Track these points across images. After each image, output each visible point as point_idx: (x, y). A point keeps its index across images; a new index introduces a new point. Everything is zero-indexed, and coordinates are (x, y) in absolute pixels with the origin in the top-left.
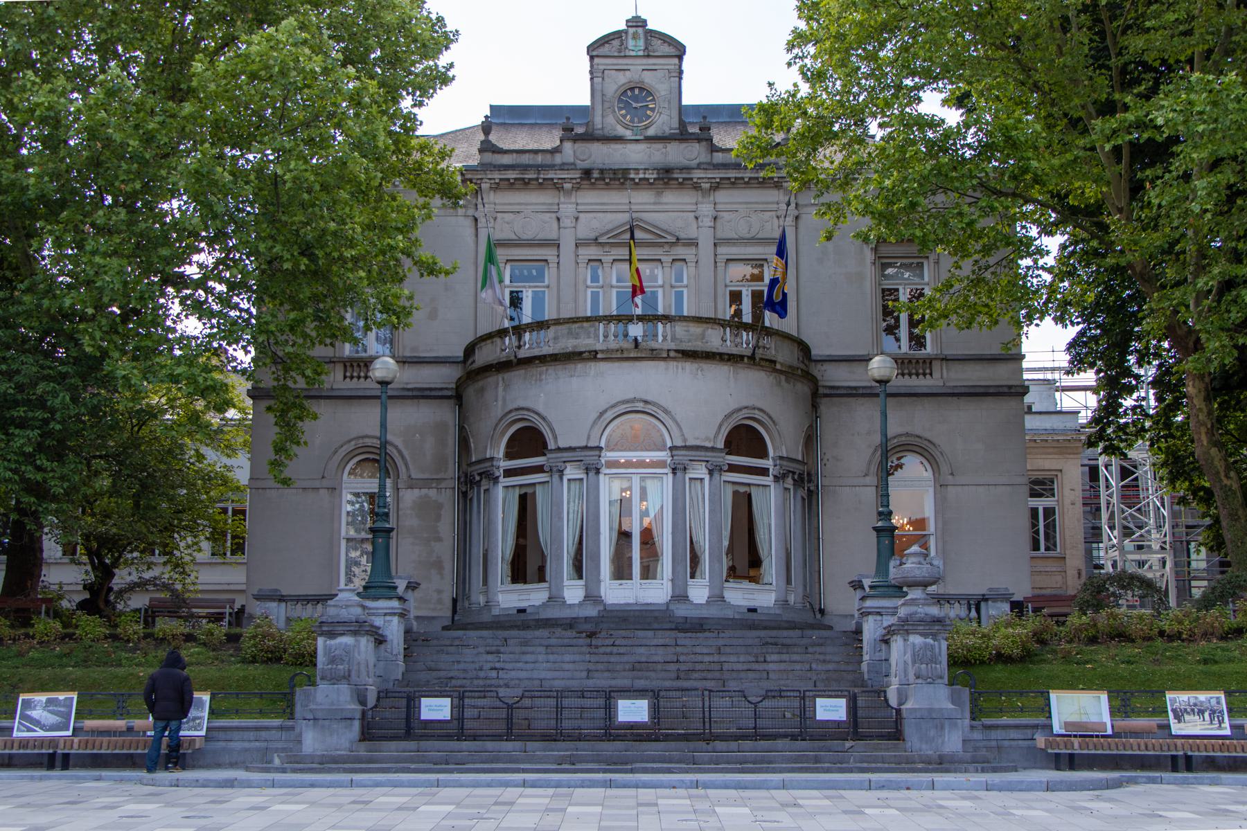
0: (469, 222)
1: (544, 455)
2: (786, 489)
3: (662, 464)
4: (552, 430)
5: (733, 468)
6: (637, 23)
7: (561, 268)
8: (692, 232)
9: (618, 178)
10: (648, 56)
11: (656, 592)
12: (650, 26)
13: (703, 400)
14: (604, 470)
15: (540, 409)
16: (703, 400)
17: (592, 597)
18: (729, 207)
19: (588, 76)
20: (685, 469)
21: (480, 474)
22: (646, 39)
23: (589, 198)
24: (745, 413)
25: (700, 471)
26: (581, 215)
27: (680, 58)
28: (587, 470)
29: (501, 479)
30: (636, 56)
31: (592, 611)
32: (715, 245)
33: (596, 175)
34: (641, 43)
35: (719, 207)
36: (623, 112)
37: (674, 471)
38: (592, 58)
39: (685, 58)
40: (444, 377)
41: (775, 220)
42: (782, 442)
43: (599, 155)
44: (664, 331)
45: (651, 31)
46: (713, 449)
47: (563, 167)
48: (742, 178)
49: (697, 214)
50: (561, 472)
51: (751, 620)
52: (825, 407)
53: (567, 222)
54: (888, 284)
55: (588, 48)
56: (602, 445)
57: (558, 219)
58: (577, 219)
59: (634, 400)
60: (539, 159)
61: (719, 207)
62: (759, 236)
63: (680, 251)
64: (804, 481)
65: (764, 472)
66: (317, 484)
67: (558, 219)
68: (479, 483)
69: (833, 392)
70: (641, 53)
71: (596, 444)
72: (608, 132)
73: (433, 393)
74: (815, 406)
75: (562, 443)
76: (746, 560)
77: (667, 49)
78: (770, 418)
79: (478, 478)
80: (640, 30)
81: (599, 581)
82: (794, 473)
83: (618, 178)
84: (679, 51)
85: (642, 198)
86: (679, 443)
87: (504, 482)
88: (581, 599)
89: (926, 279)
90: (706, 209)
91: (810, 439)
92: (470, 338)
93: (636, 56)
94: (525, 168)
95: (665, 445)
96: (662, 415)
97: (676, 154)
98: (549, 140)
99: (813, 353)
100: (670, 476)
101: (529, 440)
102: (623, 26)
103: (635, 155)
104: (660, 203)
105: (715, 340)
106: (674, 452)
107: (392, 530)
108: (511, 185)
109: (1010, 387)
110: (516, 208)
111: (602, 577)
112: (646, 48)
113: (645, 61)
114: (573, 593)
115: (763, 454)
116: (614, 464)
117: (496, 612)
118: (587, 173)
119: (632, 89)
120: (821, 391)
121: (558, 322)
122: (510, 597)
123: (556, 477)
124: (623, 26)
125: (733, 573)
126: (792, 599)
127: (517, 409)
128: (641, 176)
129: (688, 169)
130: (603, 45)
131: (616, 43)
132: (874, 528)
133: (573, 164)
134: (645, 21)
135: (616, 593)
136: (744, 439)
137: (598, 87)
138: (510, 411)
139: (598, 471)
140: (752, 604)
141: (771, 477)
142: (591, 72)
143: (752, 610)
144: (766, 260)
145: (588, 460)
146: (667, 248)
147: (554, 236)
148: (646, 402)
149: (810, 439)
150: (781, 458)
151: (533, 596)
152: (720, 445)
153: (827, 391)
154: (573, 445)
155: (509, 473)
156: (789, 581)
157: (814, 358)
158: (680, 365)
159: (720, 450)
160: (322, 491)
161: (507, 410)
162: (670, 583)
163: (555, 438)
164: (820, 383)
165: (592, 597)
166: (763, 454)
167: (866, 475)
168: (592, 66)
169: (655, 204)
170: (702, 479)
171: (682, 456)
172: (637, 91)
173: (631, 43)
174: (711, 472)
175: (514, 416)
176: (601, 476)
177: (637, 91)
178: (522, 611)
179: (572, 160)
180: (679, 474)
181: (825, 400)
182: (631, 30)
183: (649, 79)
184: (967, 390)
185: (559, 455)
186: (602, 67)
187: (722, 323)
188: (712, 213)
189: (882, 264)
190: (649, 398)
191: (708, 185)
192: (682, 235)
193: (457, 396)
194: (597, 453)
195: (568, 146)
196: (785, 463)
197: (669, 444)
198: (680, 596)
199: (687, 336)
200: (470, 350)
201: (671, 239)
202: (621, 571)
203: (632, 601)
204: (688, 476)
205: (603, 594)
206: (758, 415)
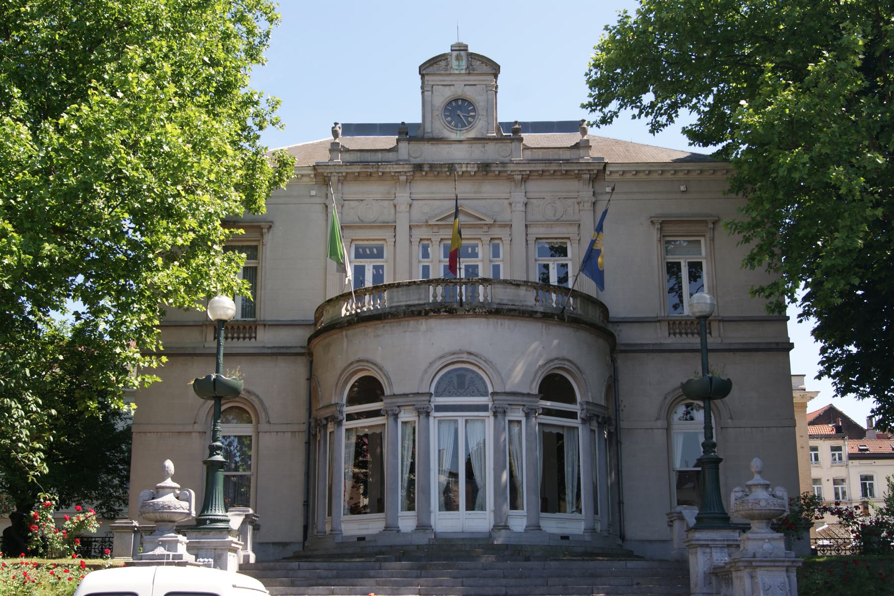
0: (320, 208)
1: (382, 400)
2: (593, 431)
3: (484, 408)
4: (388, 378)
5: (548, 412)
6: (460, 48)
7: (397, 245)
8: (506, 217)
9: (447, 171)
10: (469, 74)
11: (479, 522)
12: (470, 50)
13: (518, 355)
14: (434, 414)
15: (378, 360)
16: (518, 355)
17: (423, 527)
18: (537, 195)
19: (420, 91)
20: (505, 412)
21: (326, 419)
22: (468, 60)
23: (422, 188)
24: (557, 364)
25: (518, 415)
26: (415, 202)
27: (496, 76)
28: (419, 414)
29: (344, 422)
30: (460, 78)
31: (423, 539)
32: (526, 226)
33: (426, 168)
34: (464, 63)
35: (529, 195)
36: (449, 119)
37: (495, 414)
38: (423, 76)
39: (499, 76)
40: (296, 338)
41: (576, 205)
42: (587, 391)
43: (430, 153)
44: (485, 292)
45: (472, 54)
46: (529, 395)
47: (397, 162)
48: (548, 171)
49: (511, 200)
50: (396, 416)
51: (563, 549)
52: (620, 359)
53: (403, 207)
54: (672, 259)
55: (420, 67)
56: (432, 391)
57: (395, 206)
58: (410, 206)
59: (461, 352)
60: (379, 156)
61: (529, 195)
62: (564, 218)
63: (496, 232)
64: (608, 421)
65: (572, 415)
66: (189, 428)
67: (395, 206)
68: (325, 427)
69: (627, 349)
70: (463, 72)
71: (427, 391)
72: (436, 134)
73: (288, 351)
74: (613, 361)
75: (397, 390)
76: (553, 497)
77: (485, 69)
78: (578, 368)
79: (324, 422)
80: (463, 53)
81: (429, 512)
82: (598, 416)
83: (447, 171)
84: (495, 69)
85: (464, 189)
86: (498, 390)
87: (347, 424)
88: (415, 528)
89: (703, 253)
90: (519, 197)
91: (612, 386)
92: (321, 301)
93: (460, 78)
94: (366, 163)
95: (487, 392)
96: (483, 365)
97: (491, 153)
98: (388, 141)
99: (611, 315)
100: (492, 418)
101: (369, 389)
102: (448, 50)
103: (459, 153)
104: (480, 192)
105: (528, 298)
106: (495, 398)
107: (720, 460)
108: (357, 177)
109: (777, 344)
110: (360, 197)
111: (432, 509)
112: (468, 68)
113: (467, 78)
114: (407, 522)
115: (572, 400)
116: (439, 408)
117: (339, 539)
118: (419, 167)
119: (456, 100)
120: (618, 348)
121: (390, 286)
122: (354, 527)
123: (391, 419)
124: (448, 50)
125: (545, 508)
126: (598, 527)
127: (358, 361)
128: (464, 169)
129: (503, 164)
130: (432, 65)
131: (443, 63)
132: (205, 462)
133: (408, 160)
134: (467, 46)
135: (448, 523)
136: (554, 386)
137: (428, 99)
138: (352, 364)
139: (428, 415)
140: (566, 532)
141: (579, 420)
142: (422, 88)
143: (565, 538)
144: (569, 238)
145: (419, 405)
146: (485, 229)
147: (391, 218)
148: (470, 353)
149: (612, 386)
150: (588, 403)
151: (369, 525)
152: (535, 390)
153: (623, 348)
154: (407, 392)
155: (350, 417)
156: (596, 513)
157: (610, 320)
158: (499, 321)
159: (535, 396)
160: (194, 434)
161: (349, 362)
162: (492, 515)
163: (390, 384)
164: (618, 341)
165: (423, 527)
166: (572, 400)
167: (657, 419)
168: (423, 83)
169: (475, 192)
170: (519, 422)
171: (502, 401)
172: (460, 102)
173: (454, 63)
174: (527, 416)
175: (355, 367)
176: (431, 419)
177: (460, 102)
178: (361, 539)
179: (406, 157)
180: (500, 416)
181: (621, 356)
182: (455, 53)
183: (469, 93)
184: (741, 347)
185: (394, 400)
186: (432, 83)
187: (534, 286)
188: (524, 200)
189: (666, 242)
190: (472, 350)
191: (520, 177)
192: (499, 218)
193: (307, 353)
194: (427, 398)
195: (403, 146)
196: (590, 407)
197: (490, 390)
198: (501, 526)
199: (503, 295)
200: (320, 311)
201: (489, 221)
202: (449, 504)
203: (459, 530)
204: (508, 418)
205: (432, 523)
206: (567, 365)
